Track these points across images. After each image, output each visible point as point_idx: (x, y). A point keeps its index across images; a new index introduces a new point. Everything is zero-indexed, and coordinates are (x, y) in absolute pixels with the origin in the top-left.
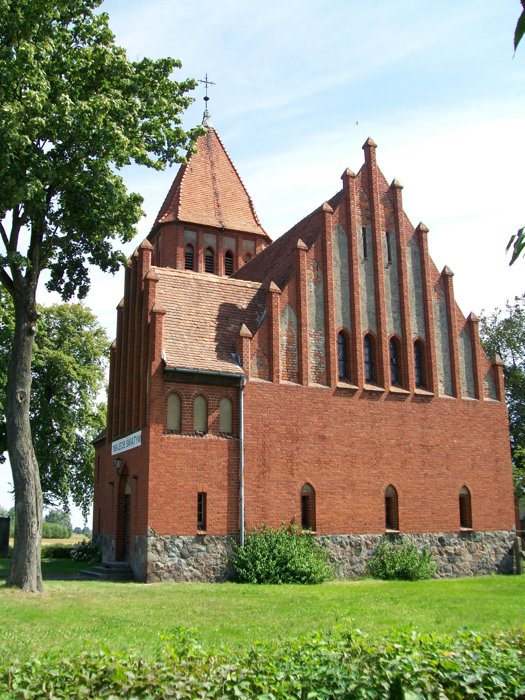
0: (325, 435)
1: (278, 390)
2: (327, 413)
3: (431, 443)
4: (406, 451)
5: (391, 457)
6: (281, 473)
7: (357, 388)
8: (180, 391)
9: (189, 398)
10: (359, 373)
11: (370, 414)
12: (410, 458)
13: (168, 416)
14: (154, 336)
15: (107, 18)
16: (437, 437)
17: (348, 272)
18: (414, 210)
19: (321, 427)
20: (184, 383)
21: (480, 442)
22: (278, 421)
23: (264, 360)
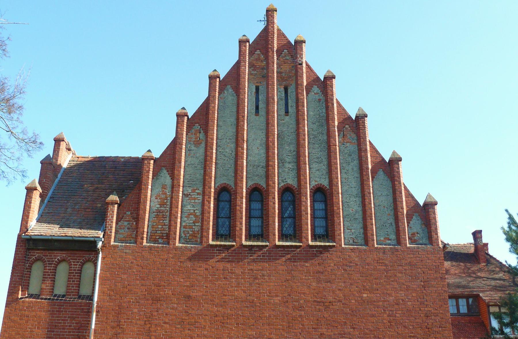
0: (191, 294)
1: (140, 251)
2: (195, 272)
3: (331, 299)
4: (294, 308)
5: (274, 316)
6: (137, 334)
7: (301, 244)
8: (44, 257)
9: (52, 264)
10: (238, 228)
11: (249, 270)
12: (300, 316)
13: (31, 282)
14: (301, 227)
15: (334, 78)
16: (338, 292)
17: (234, 130)
18: (316, 59)
19: (187, 286)
20: (48, 250)
21: (402, 294)
22: (138, 282)
23: (133, 224)
